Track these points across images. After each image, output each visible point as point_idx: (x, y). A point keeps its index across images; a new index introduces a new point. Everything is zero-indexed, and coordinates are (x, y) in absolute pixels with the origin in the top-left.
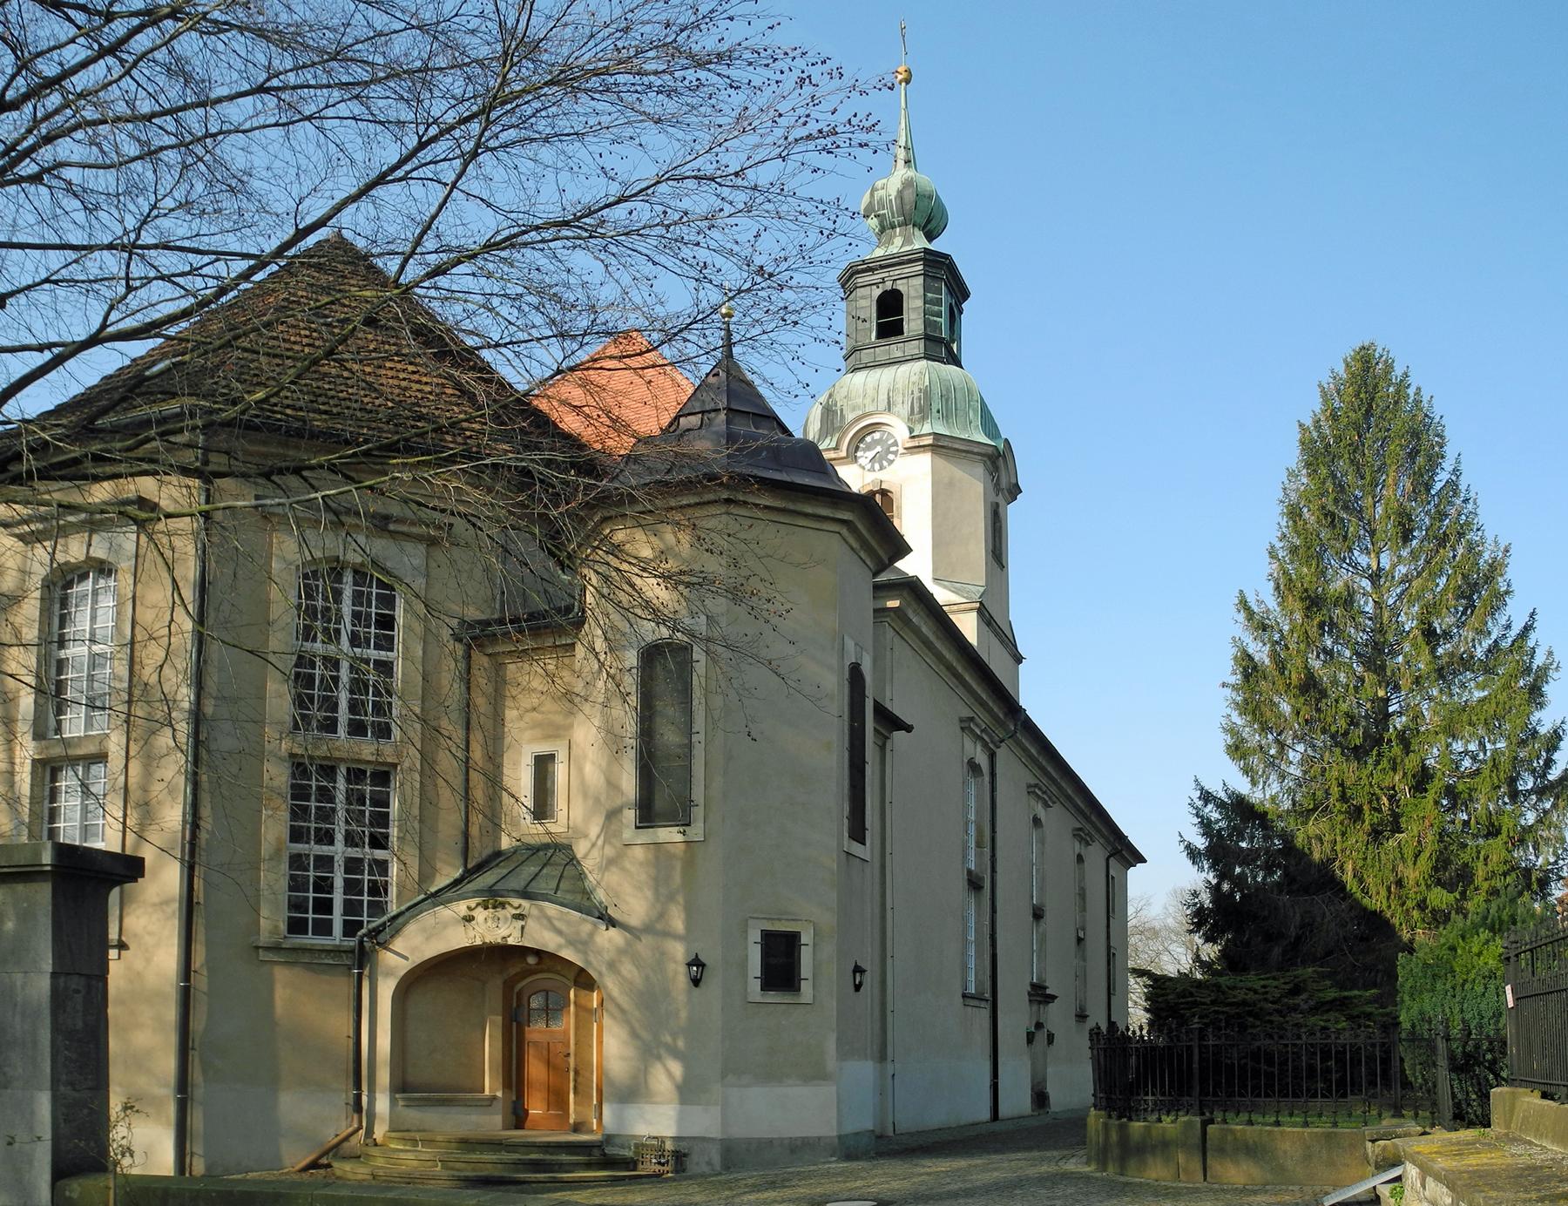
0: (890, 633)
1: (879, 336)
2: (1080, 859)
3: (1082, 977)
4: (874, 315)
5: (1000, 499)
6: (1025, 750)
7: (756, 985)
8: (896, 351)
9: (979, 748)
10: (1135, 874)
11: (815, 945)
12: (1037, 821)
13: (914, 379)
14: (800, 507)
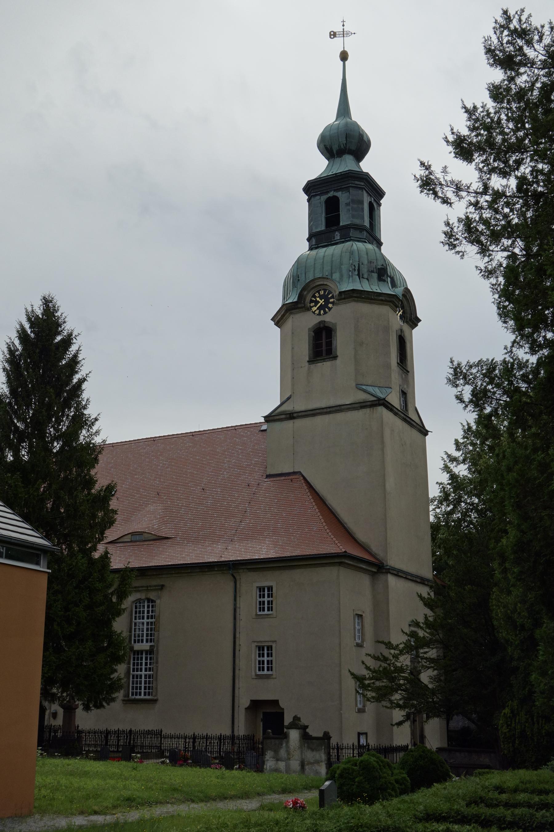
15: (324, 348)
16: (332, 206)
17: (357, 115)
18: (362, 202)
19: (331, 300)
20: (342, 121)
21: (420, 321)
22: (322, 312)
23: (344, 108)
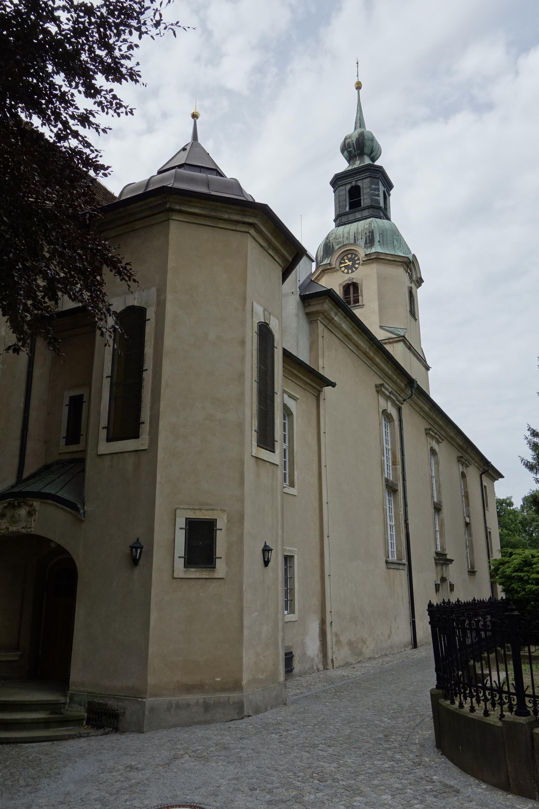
0: (321, 327)
1: (350, 208)
2: (463, 475)
3: (470, 547)
4: (348, 198)
5: (413, 285)
6: (421, 408)
7: (180, 563)
8: (358, 215)
9: (389, 404)
10: (498, 483)
11: (228, 529)
12: (433, 452)
13: (366, 226)
14: (238, 228)
15: (352, 299)
16: (355, 194)
17: (369, 127)
18: (378, 190)
19: (357, 262)
20: (359, 130)
21: (423, 281)
22: (350, 271)
23: (360, 122)
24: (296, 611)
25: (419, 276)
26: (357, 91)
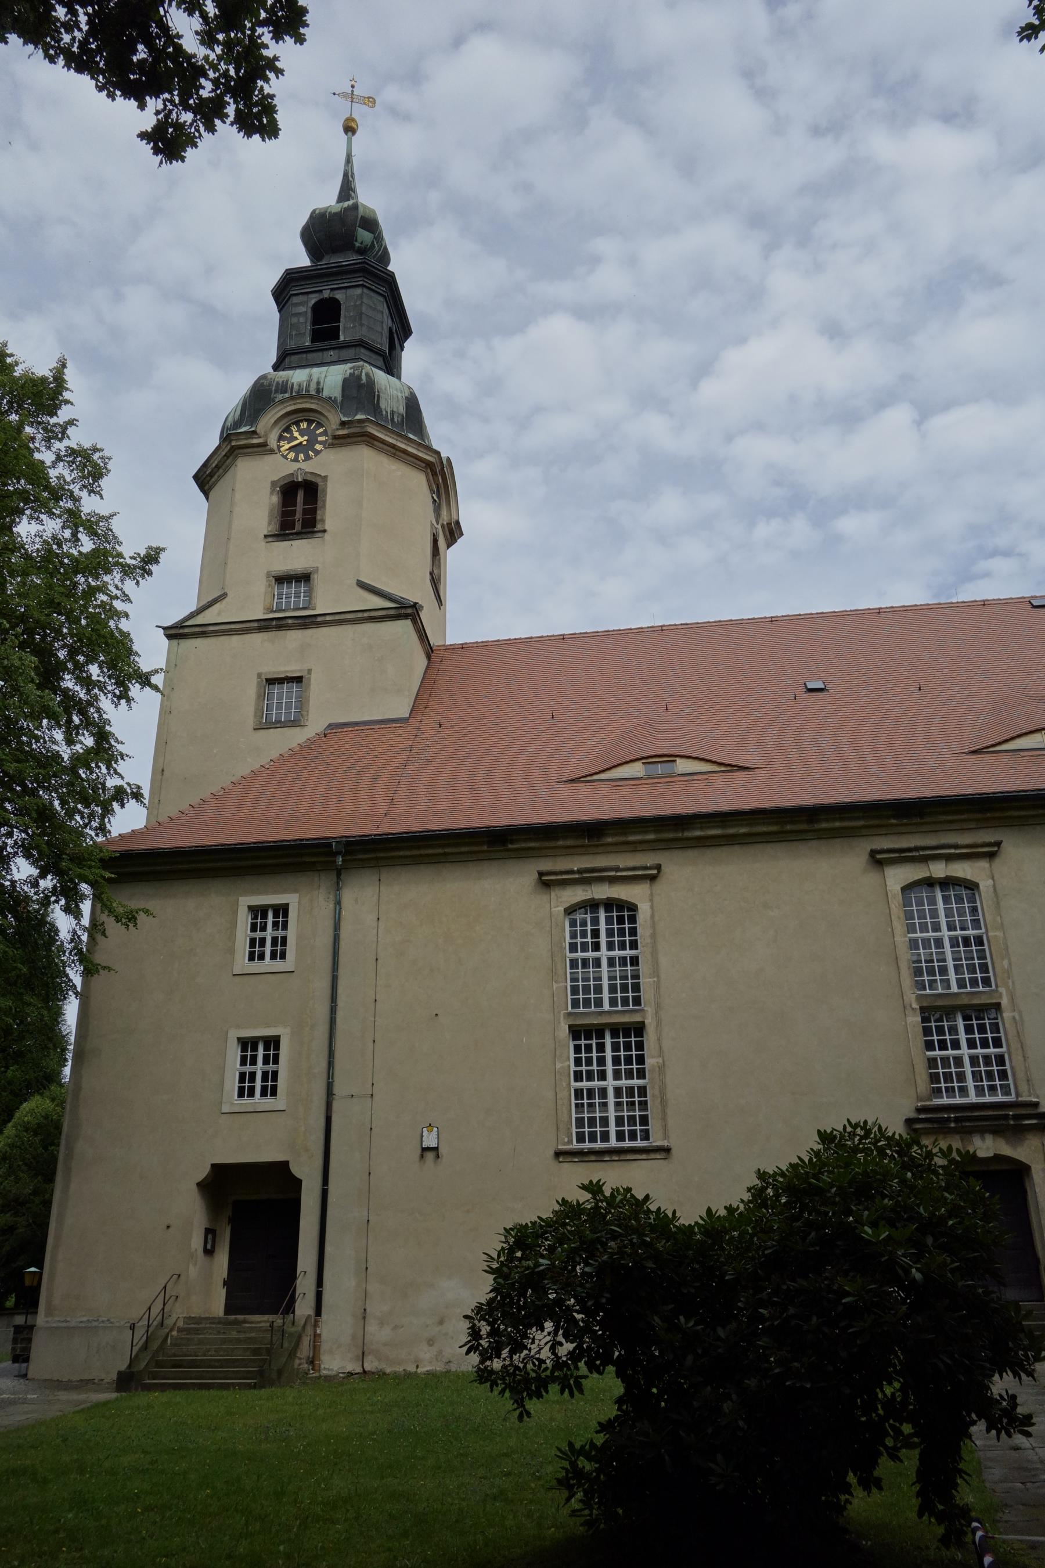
22: (301, 456)
23: (347, 190)
24: (281, 373)
25: (455, 517)
26: (344, 137)
